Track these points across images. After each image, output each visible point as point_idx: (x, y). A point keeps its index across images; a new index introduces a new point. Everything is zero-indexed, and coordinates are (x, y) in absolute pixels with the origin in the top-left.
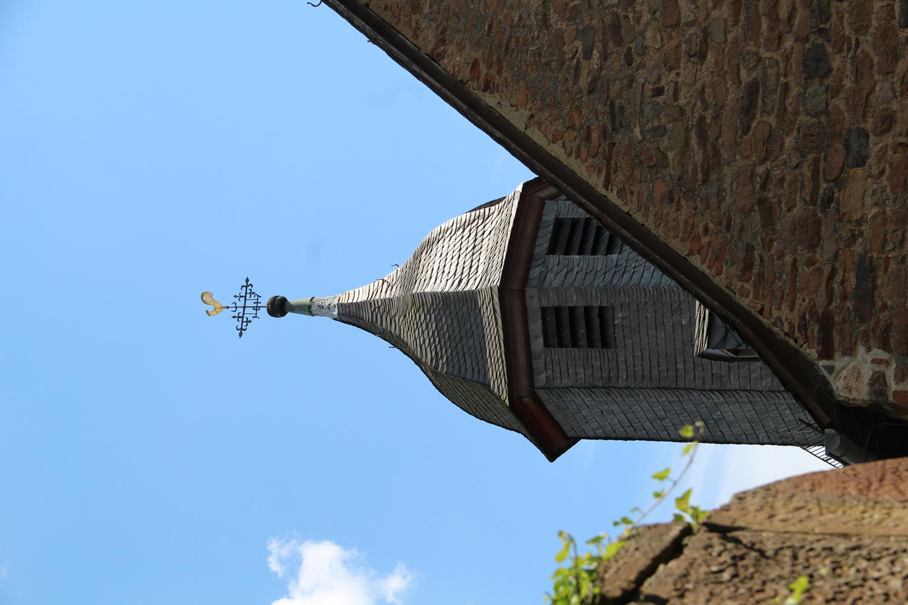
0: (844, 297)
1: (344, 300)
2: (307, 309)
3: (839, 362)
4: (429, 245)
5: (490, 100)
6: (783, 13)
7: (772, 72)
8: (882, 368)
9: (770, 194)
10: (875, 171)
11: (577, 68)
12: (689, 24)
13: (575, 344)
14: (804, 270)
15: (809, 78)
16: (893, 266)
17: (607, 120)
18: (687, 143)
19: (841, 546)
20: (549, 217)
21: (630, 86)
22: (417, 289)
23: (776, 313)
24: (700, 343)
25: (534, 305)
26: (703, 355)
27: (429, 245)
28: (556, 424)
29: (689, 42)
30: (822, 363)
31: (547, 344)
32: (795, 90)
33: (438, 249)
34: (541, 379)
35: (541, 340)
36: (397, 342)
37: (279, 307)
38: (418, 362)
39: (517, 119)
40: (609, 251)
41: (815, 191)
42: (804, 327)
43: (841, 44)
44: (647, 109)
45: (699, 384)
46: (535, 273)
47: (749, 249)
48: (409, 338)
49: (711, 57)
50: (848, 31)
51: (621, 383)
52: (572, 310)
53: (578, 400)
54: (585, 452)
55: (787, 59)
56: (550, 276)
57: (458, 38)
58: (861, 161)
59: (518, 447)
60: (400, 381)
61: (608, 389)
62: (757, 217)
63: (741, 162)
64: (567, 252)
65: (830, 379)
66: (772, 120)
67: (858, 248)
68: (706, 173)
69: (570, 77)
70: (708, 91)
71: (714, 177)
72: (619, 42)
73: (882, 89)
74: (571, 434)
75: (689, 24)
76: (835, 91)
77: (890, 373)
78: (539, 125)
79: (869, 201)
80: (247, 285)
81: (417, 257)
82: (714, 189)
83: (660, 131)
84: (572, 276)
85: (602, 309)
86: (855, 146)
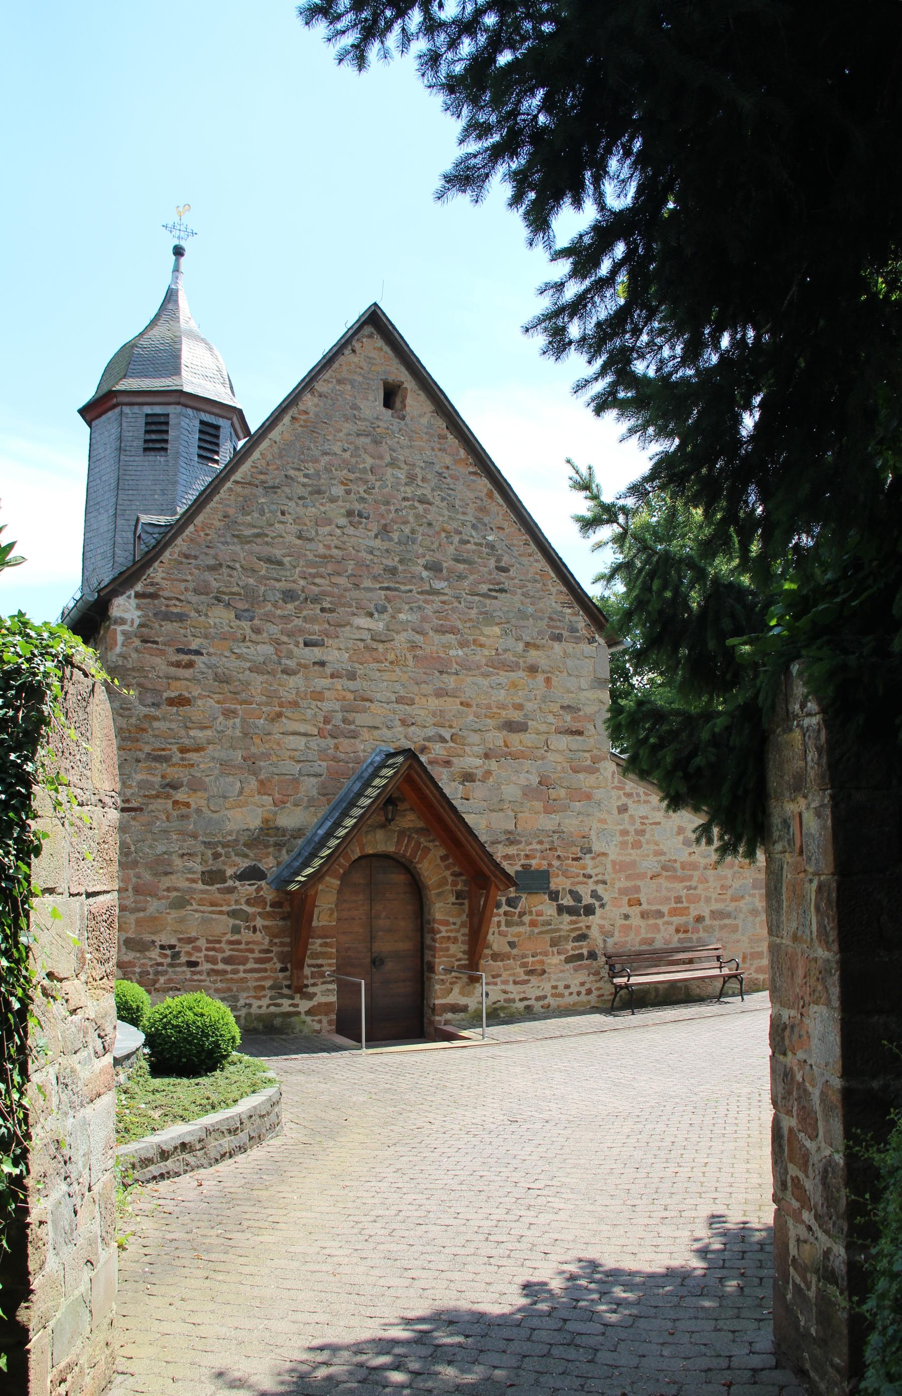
0: (167, 606)
1: (180, 294)
2: (176, 269)
3: (133, 602)
4: (211, 349)
5: (287, 419)
6: (317, 580)
7: (288, 573)
8: (129, 623)
9: (224, 570)
10: (232, 624)
11: (299, 470)
12: (317, 532)
13: (147, 432)
14: (183, 585)
15: (283, 593)
16: (182, 631)
17: (270, 484)
18: (254, 527)
19: (88, 734)
20: (221, 422)
21: (288, 498)
22: (185, 341)
23: (160, 570)
24: (145, 519)
25: (170, 410)
26: (138, 520)
27: (211, 349)
28: (99, 416)
29: (308, 530)
30: (133, 593)
31: (147, 415)
32: (277, 585)
33: (207, 354)
34: (126, 410)
35: (150, 412)
36: (154, 323)
37: (178, 252)
38: (141, 334)
39: (275, 434)
40: (200, 456)
41: (224, 593)
42: (152, 584)
43: (299, 609)
44: (274, 507)
45: (120, 502)
46: (190, 411)
47: (196, 557)
48: (155, 332)
49: (299, 542)
50: (305, 613)
51: (122, 458)
52: (167, 432)
53: (113, 431)
54: (84, 429)
55: (294, 582)
56: (187, 421)
57: (321, 404)
58: (238, 617)
59: (88, 393)
60: (128, 323)
61: (120, 449)
62: (212, 562)
63: (242, 555)
64: (201, 431)
65: (124, 596)
66: (263, 572)
67: (193, 614)
68: (237, 536)
69: (295, 466)
70: (281, 540)
71: (235, 540)
72: (311, 493)
73: (274, 629)
74: (94, 424)
75: (317, 532)
76: (275, 606)
77: (126, 627)
78: (271, 446)
79: (217, 620)
80: (194, 234)
81: (203, 340)
82: (229, 540)
83: (262, 513)
84: (186, 433)
85: (166, 449)
86: (246, 614)
